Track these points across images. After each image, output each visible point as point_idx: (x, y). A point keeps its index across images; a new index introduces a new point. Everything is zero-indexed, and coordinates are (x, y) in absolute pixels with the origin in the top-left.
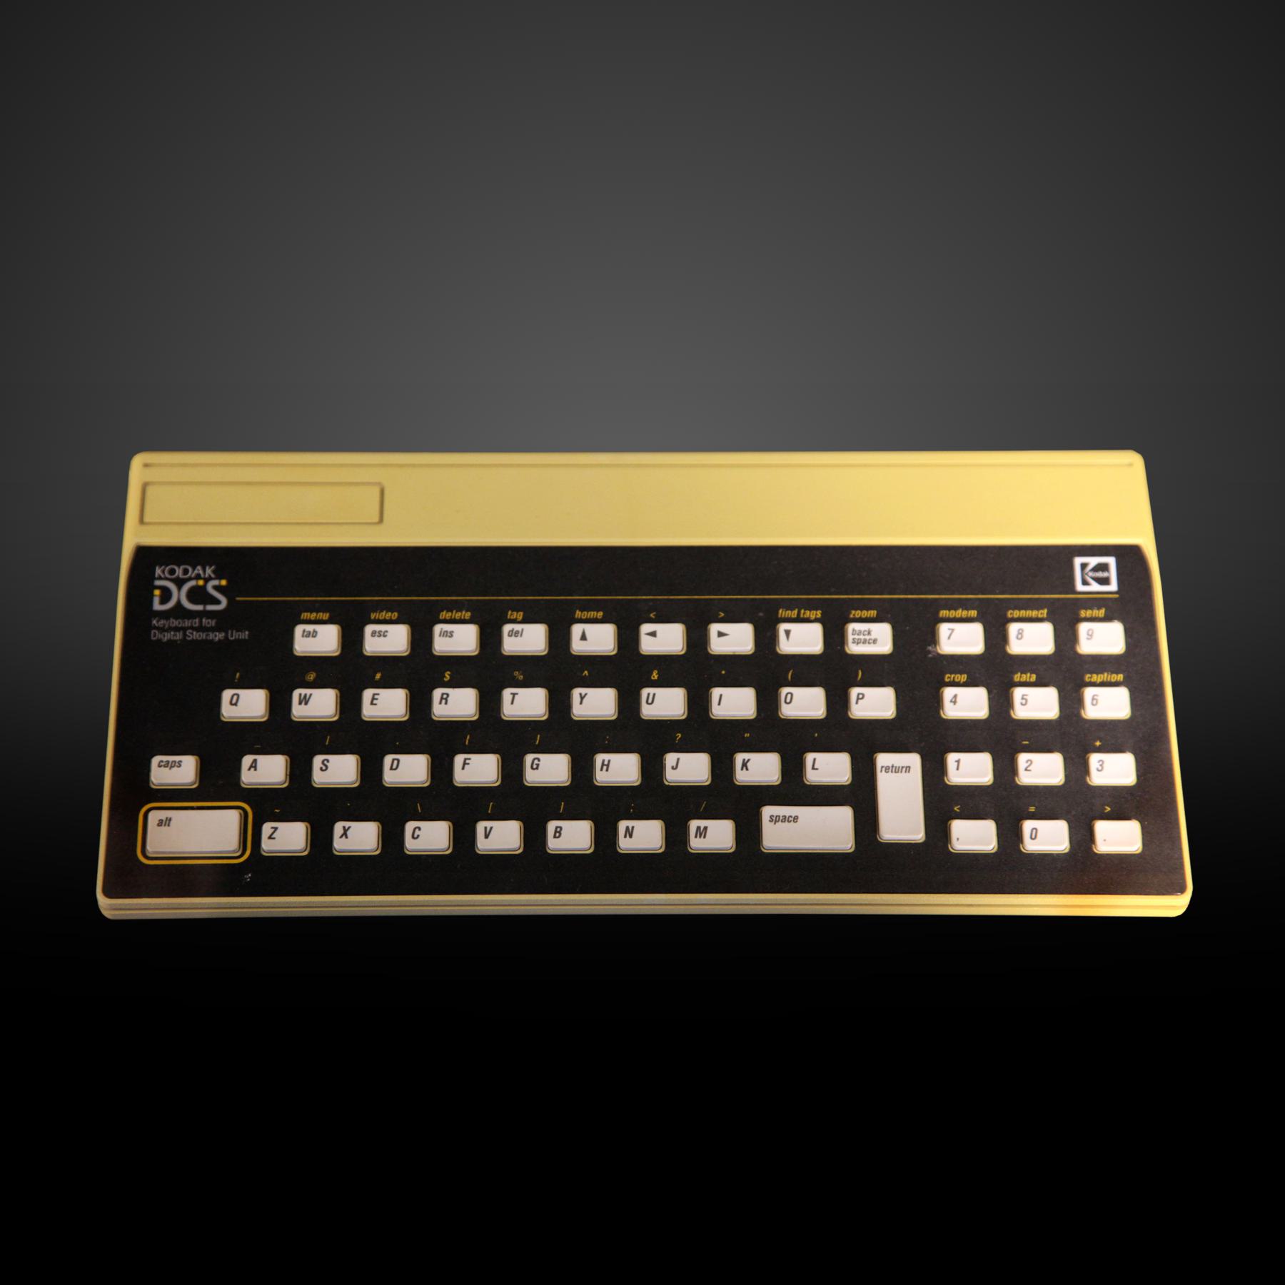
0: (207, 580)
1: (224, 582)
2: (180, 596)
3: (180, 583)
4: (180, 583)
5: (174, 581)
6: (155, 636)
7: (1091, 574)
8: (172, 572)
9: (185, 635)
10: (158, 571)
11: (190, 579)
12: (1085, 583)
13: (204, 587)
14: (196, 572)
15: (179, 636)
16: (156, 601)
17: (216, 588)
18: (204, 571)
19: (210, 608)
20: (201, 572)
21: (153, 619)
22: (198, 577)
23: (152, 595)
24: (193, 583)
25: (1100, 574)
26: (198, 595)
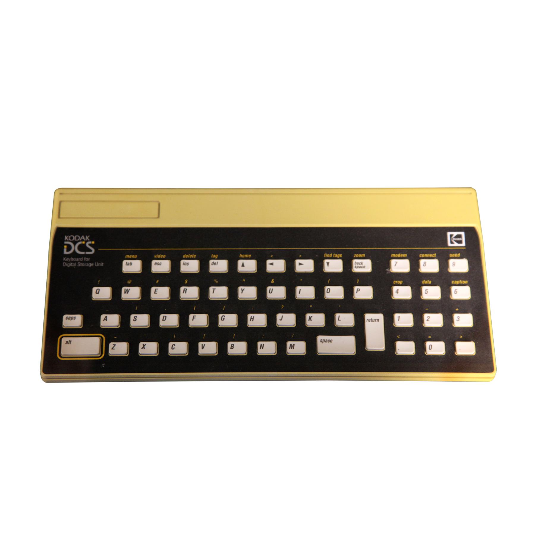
0: (86, 242)
1: (93, 242)
2: (75, 248)
3: (75, 243)
4: (75, 243)
5: (73, 242)
6: (64, 265)
7: (454, 239)
8: (72, 238)
9: (77, 264)
10: (66, 238)
11: (79, 241)
12: (452, 243)
13: (85, 244)
14: (82, 238)
15: (75, 265)
16: (65, 250)
17: (90, 245)
19: (88, 253)
20: (84, 238)
22: (82, 240)
23: (63, 248)
24: (80, 243)
25: (458, 239)
26: (82, 248)
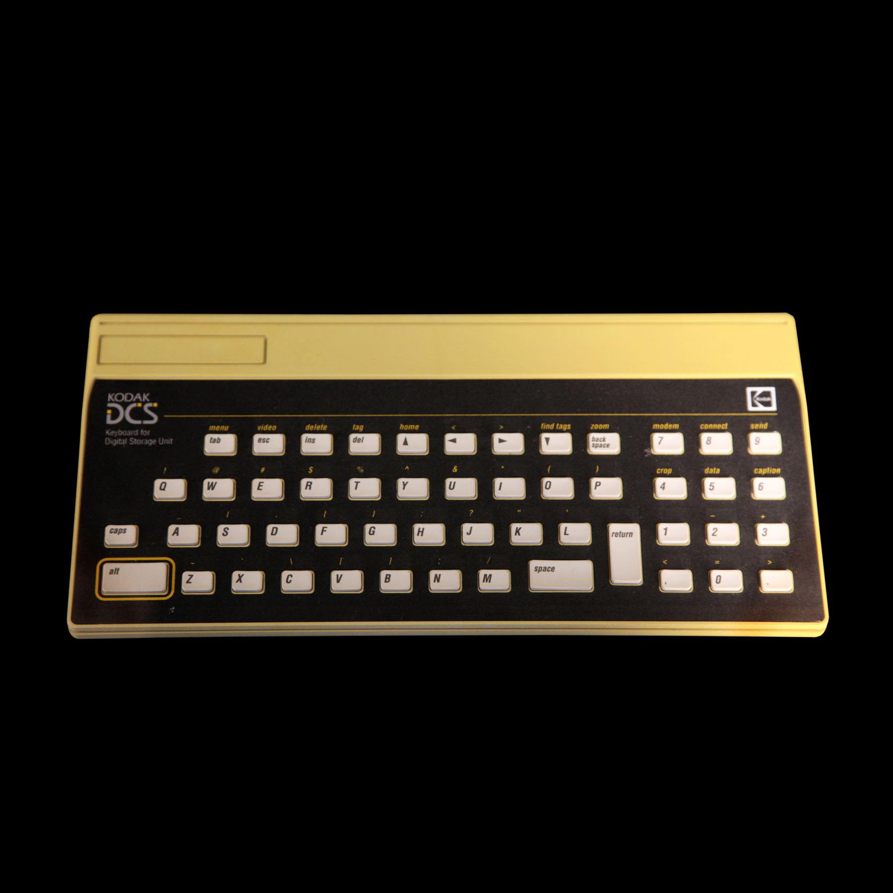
0: (144, 403)
1: (155, 405)
2: (125, 414)
3: (125, 405)
4: (125, 405)
5: (121, 404)
6: (107, 442)
7: (758, 399)
8: (120, 397)
10: (110, 397)
11: (132, 402)
12: (754, 405)
13: (142, 408)
14: (136, 397)
15: (124, 442)
16: (109, 417)
17: (150, 408)
18: (142, 397)
19: (146, 422)
20: (140, 398)
21: (106, 430)
22: (138, 401)
23: (106, 414)
24: (134, 405)
25: (765, 399)
26: (137, 413)
